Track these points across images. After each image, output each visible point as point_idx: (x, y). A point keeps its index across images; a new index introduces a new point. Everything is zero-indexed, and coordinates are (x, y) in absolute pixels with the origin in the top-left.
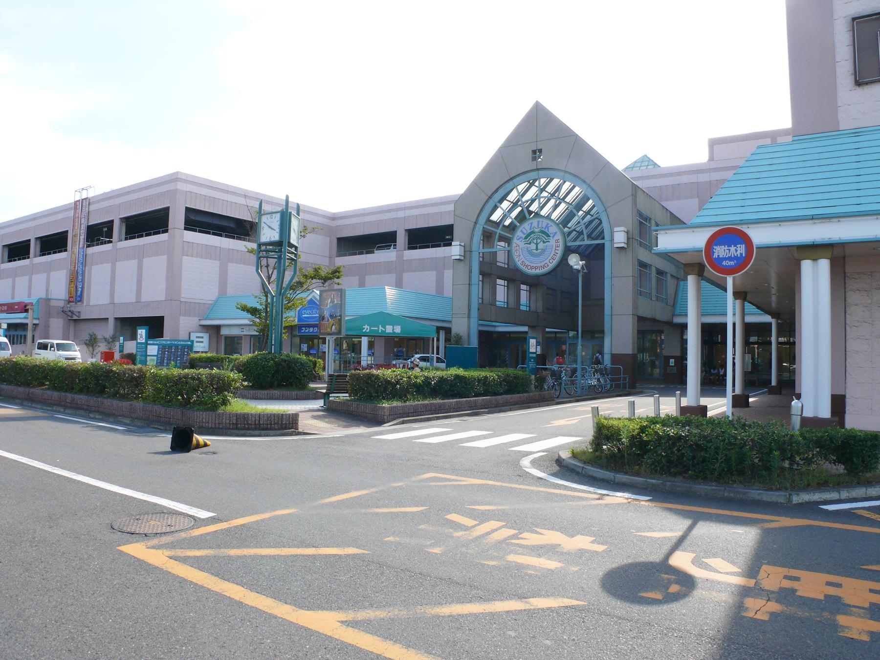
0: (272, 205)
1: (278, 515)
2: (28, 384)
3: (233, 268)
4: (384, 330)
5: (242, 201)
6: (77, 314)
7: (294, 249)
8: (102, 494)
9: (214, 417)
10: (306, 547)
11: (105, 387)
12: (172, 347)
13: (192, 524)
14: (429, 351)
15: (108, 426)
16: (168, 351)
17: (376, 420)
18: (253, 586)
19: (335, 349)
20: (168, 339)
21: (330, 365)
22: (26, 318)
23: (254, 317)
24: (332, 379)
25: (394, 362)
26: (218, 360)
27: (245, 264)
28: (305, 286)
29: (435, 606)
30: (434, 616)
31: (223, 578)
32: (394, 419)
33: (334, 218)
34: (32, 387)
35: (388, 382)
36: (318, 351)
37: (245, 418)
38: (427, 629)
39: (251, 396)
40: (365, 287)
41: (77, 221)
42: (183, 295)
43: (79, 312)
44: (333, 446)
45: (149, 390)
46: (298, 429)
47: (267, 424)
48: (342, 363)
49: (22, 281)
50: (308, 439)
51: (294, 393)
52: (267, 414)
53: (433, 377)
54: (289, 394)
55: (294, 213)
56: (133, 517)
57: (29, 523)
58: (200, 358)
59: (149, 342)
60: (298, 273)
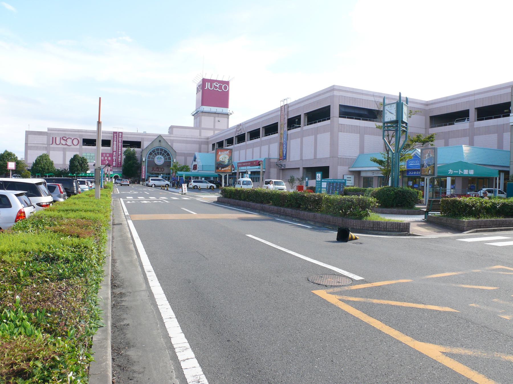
0: (389, 99)
1: (400, 282)
2: (262, 202)
3: (368, 138)
4: (462, 172)
5: (372, 99)
6: (284, 166)
7: (405, 124)
8: (302, 261)
9: (360, 223)
10: (418, 303)
11: (301, 205)
12: (334, 183)
13: (351, 283)
15: (303, 225)
16: (332, 186)
17: (459, 229)
18: (387, 322)
19: (430, 185)
20: (332, 178)
21: (427, 194)
22: (259, 168)
23: (381, 166)
24: (430, 203)
25: (469, 193)
26: (360, 190)
27: (374, 135)
28: (411, 147)
29: (507, 355)
30: (507, 361)
31: (369, 315)
32: (470, 229)
33: (427, 104)
34: (264, 204)
35: (467, 206)
36: (419, 186)
37: (378, 224)
38: (503, 369)
39: (380, 212)
40: (448, 146)
41: (282, 117)
42: (339, 154)
43: (285, 165)
44: (432, 244)
45: (324, 206)
46: (409, 232)
47: (391, 228)
48: (434, 193)
49: (257, 150)
50: (416, 238)
51: (406, 211)
52: (391, 223)
53: (498, 203)
54: (403, 211)
55: (405, 103)
56: (319, 276)
57: (267, 273)
58: (350, 190)
59: (323, 181)
60: (408, 140)
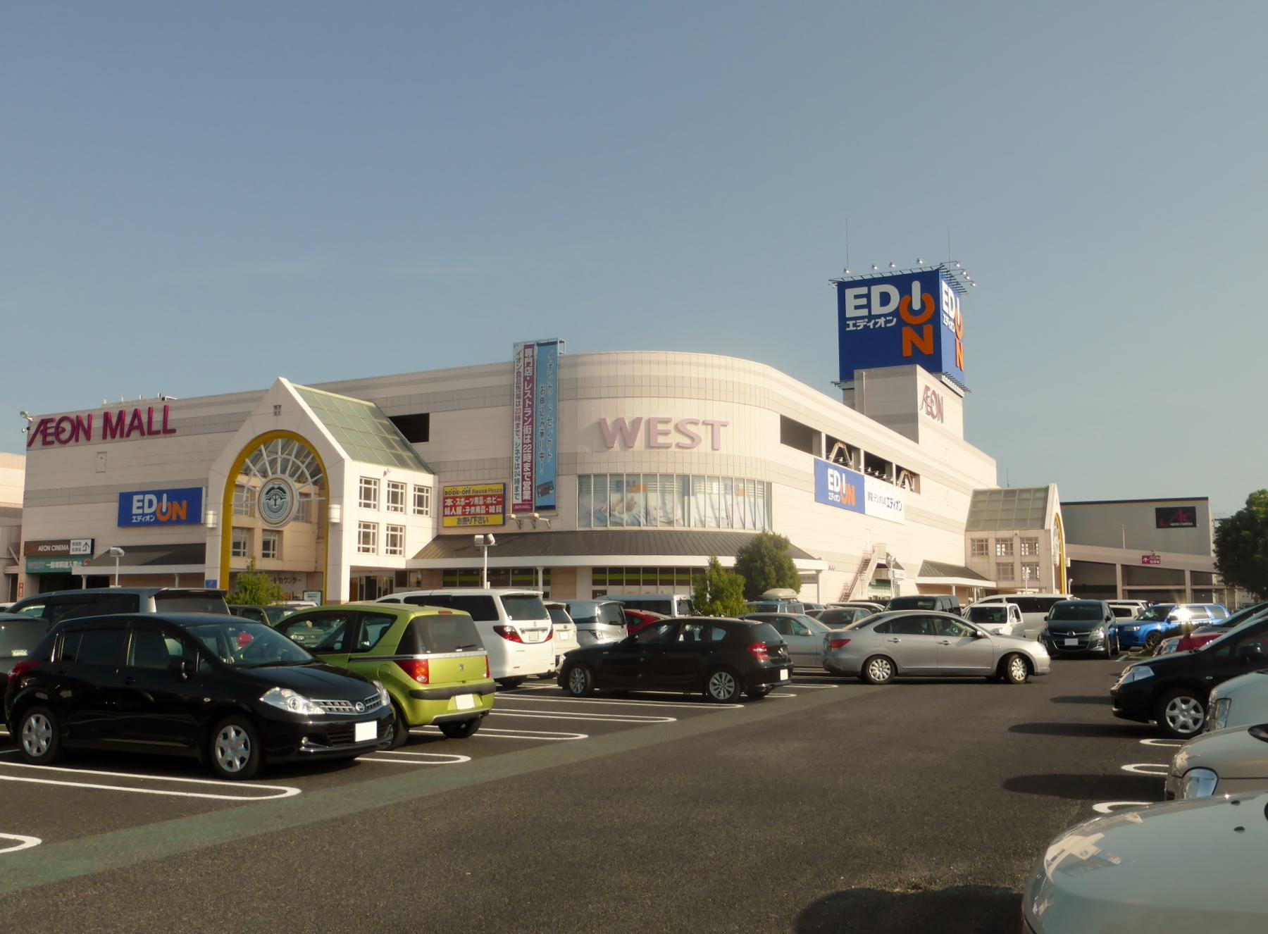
14: (25, 545)
